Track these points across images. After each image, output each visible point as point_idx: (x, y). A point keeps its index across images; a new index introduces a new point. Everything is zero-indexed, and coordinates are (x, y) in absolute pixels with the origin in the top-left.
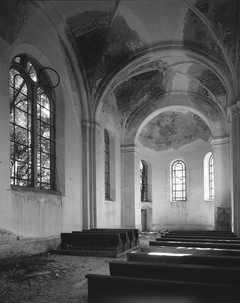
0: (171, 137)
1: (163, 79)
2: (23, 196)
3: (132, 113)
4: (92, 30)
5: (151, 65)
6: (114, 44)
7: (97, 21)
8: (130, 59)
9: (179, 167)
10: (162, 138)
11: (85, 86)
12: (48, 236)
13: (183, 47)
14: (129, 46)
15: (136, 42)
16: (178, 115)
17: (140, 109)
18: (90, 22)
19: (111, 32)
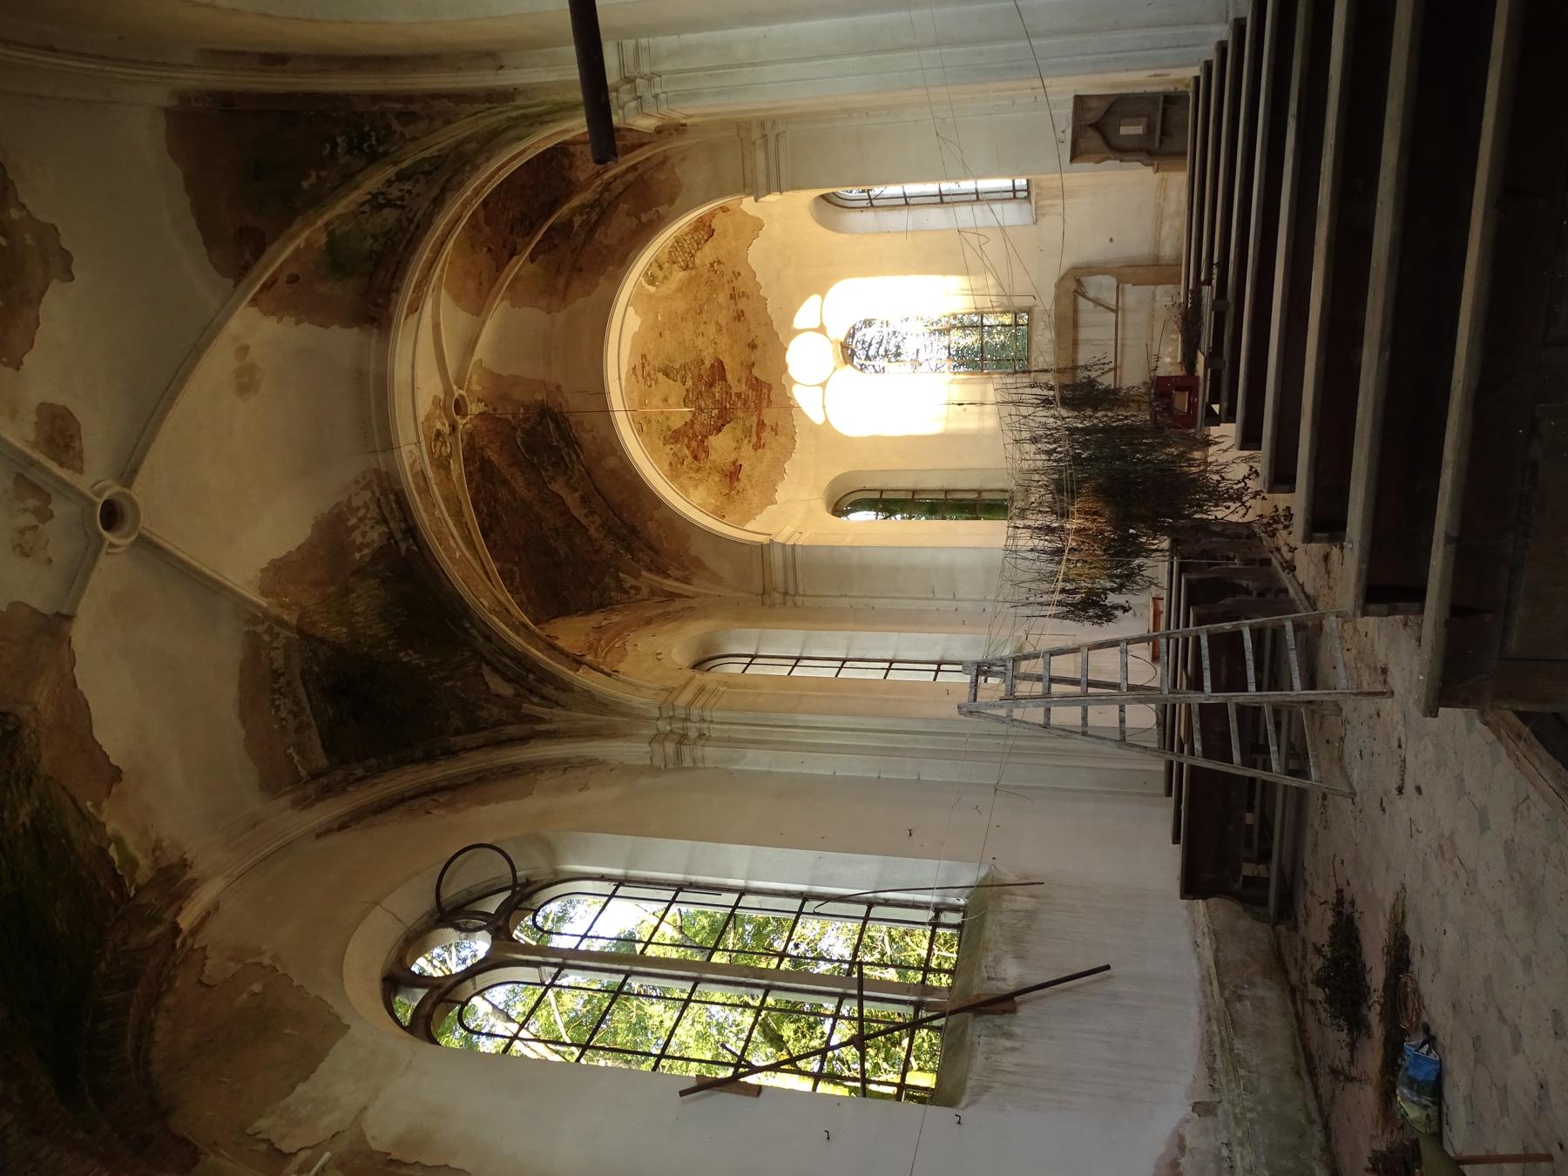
0: (736, 380)
2: (987, 1059)
3: (629, 550)
4: (304, 698)
5: (442, 464)
6: (359, 609)
7: (274, 672)
8: (414, 548)
11: (511, 741)
12: (1194, 962)
13: (379, 328)
14: (365, 552)
15: (353, 521)
16: (646, 352)
17: (611, 513)
18: (277, 702)
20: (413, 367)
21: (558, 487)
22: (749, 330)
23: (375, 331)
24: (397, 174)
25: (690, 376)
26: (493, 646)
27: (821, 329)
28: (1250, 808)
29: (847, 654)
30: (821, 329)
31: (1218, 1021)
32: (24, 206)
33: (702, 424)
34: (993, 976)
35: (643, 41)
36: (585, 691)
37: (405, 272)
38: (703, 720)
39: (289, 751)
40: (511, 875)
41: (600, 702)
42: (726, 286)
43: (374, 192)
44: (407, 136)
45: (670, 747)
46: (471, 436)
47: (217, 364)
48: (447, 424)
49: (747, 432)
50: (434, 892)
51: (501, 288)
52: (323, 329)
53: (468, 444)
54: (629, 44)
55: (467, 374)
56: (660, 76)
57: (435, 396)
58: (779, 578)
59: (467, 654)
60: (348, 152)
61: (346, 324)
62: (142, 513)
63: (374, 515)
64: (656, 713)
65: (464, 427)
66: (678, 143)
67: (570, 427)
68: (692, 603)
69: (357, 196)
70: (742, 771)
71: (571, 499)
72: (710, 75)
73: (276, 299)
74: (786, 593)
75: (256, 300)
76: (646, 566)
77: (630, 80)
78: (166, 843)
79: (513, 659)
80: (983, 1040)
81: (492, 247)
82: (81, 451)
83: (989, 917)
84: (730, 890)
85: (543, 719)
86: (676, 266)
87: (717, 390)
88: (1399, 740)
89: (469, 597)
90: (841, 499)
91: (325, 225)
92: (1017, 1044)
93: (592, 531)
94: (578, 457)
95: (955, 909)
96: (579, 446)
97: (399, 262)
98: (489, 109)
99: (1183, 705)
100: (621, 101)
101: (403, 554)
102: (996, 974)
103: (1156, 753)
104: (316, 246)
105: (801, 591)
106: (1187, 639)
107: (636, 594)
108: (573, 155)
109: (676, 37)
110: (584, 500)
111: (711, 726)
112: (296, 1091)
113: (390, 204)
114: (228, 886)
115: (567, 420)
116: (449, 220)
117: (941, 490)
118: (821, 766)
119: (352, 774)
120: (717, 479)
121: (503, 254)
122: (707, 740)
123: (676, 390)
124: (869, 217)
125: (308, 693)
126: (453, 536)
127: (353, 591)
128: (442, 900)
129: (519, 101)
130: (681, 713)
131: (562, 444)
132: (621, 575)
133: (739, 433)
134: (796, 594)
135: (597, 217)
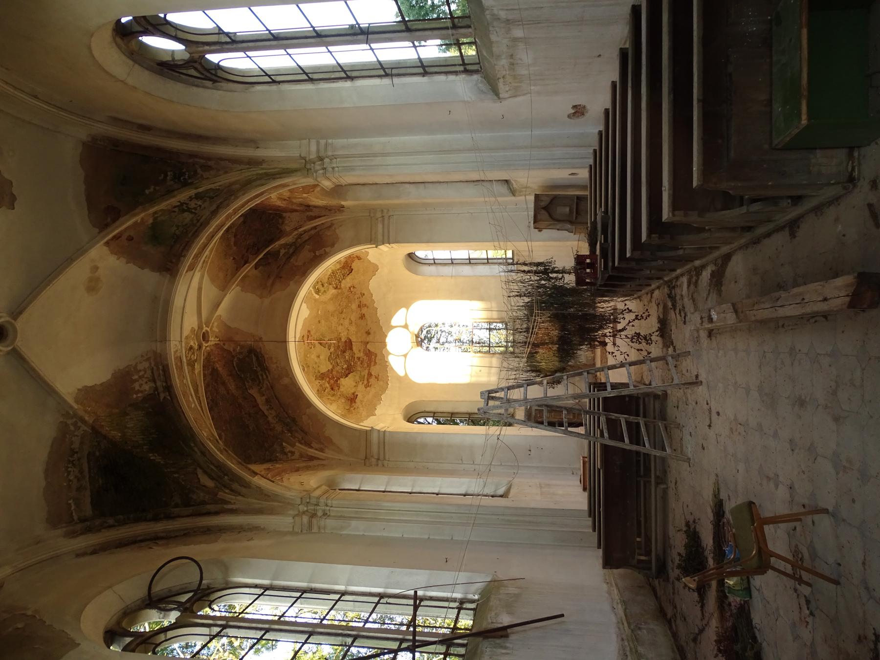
1: (225, 347)
3: (290, 431)
4: (87, 470)
8: (169, 398)
9: (411, 644)
10: (359, 372)
11: (209, 514)
15: (135, 377)
18: (69, 469)
19: (103, 426)
20: (185, 300)
21: (253, 392)
22: (367, 325)
23: (169, 276)
24: (196, 194)
26: (205, 458)
27: (406, 326)
28: (639, 536)
29: (412, 490)
30: (406, 326)
31: (628, 641)
33: (337, 372)
34: (495, 621)
35: (330, 141)
36: (257, 487)
37: (190, 247)
38: (327, 505)
39: (70, 502)
41: (266, 495)
43: (182, 201)
44: (205, 177)
45: (305, 519)
46: (209, 354)
47: (78, 271)
48: (197, 344)
49: (362, 378)
53: (206, 358)
54: (323, 142)
55: (211, 321)
56: (336, 159)
57: (193, 328)
59: (190, 461)
61: (153, 269)
62: (19, 335)
63: (149, 376)
64: (298, 501)
65: (206, 348)
66: (339, 217)
67: (264, 360)
69: (173, 201)
70: (349, 535)
71: (260, 400)
72: (361, 160)
73: (119, 245)
74: (378, 459)
75: (108, 243)
76: (299, 441)
77: (321, 159)
79: (216, 467)
80: (488, 650)
81: (236, 257)
83: (493, 596)
84: (335, 592)
85: (230, 502)
86: (331, 286)
87: (347, 355)
88: (707, 401)
90: (412, 416)
91: (154, 213)
92: (508, 652)
93: (270, 418)
94: (267, 377)
95: (472, 601)
97: (188, 242)
100: (316, 169)
101: (161, 400)
102: (496, 621)
103: (584, 437)
105: (387, 458)
106: (594, 399)
107: (291, 456)
108: (284, 218)
109: (346, 140)
110: (267, 401)
111: (331, 508)
113: (189, 210)
114: (13, 574)
115: (264, 357)
116: (219, 224)
117: (467, 413)
118: (395, 532)
120: (343, 401)
121: (241, 262)
122: (328, 516)
123: (325, 353)
124: (433, 268)
125: (89, 468)
126: (192, 396)
128: (152, 592)
130: (313, 501)
131: (259, 369)
133: (357, 378)
134: (385, 459)
135: (293, 251)
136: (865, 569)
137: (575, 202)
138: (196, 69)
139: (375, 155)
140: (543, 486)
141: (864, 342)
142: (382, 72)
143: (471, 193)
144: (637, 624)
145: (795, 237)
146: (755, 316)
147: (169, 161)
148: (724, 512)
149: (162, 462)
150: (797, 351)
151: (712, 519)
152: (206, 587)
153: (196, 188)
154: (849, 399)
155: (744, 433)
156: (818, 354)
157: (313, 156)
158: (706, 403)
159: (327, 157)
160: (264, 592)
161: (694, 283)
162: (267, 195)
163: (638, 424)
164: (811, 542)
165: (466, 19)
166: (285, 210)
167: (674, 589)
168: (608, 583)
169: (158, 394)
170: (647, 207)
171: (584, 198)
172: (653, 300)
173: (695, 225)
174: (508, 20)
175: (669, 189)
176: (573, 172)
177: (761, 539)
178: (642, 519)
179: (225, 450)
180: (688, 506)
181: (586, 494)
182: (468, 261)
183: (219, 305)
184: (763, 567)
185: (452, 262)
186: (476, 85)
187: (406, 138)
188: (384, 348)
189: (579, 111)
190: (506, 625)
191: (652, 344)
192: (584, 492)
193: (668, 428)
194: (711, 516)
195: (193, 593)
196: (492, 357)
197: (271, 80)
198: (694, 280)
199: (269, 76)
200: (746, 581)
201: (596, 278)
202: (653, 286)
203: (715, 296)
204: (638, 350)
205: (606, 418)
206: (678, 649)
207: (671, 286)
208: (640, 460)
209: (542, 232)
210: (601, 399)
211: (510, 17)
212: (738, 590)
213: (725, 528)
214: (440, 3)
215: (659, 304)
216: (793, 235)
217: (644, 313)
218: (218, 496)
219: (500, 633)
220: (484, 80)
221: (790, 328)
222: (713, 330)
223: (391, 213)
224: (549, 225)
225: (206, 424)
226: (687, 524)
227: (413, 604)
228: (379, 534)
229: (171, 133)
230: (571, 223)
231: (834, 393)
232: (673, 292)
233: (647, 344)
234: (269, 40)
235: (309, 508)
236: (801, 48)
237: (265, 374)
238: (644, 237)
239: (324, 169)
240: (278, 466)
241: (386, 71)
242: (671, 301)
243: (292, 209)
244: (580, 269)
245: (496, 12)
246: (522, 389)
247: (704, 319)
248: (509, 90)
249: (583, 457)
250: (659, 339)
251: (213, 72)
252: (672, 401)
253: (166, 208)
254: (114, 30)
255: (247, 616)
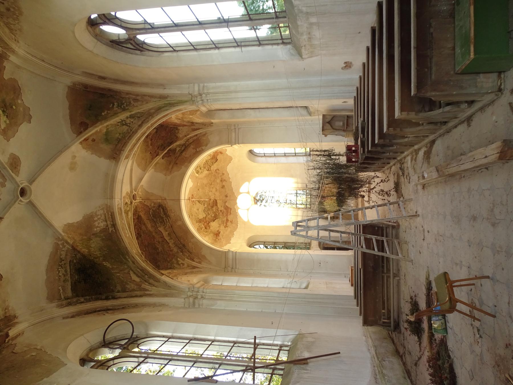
1: (145, 203)
3: (182, 252)
4: (69, 270)
7: (61, 259)
8: (114, 231)
11: (136, 296)
13: (116, 161)
17: (177, 240)
18: (59, 270)
20: (123, 175)
21: (161, 229)
23: (114, 162)
24: (130, 115)
25: (206, 203)
28: (384, 309)
30: (248, 193)
31: (377, 367)
32: (23, 100)
33: (209, 218)
35: (206, 84)
36: (164, 282)
38: (203, 292)
39: (59, 288)
40: (131, 334)
42: (220, 177)
43: (122, 119)
45: (191, 300)
47: (65, 159)
49: (223, 222)
50: (103, 336)
51: (152, 165)
52: (99, 158)
53: (135, 209)
54: (201, 85)
57: (127, 192)
58: (230, 262)
59: (126, 267)
60: (117, 107)
61: (106, 158)
63: (103, 218)
64: (187, 290)
66: (210, 129)
67: (167, 211)
68: (201, 270)
70: (215, 309)
71: (165, 234)
74: (232, 268)
77: (201, 95)
78: (10, 308)
79: (141, 270)
80: (296, 371)
82: (20, 170)
84: (208, 340)
85: (148, 290)
87: (214, 208)
89: (129, 248)
93: (170, 244)
96: (170, 218)
97: (125, 142)
98: (159, 100)
99: (360, 252)
101: (110, 232)
104: (102, 132)
105: (237, 268)
106: (358, 225)
111: (206, 294)
112: (43, 380)
113: (126, 124)
114: (29, 327)
117: (283, 242)
118: (242, 308)
119: (80, 300)
120: (212, 235)
123: (201, 207)
124: (264, 159)
125: (70, 269)
127: (92, 240)
128: (105, 339)
129: (168, 99)
130: (196, 290)
131: (164, 216)
132: (178, 259)
133: (220, 222)
134: (236, 268)
136: (509, 306)
137: (346, 118)
138: (131, 44)
139: (231, 92)
140: (328, 283)
141: (508, 179)
142: (235, 44)
143: (285, 114)
144: (383, 358)
145: (470, 126)
146: (448, 172)
147: (115, 97)
148: (432, 288)
149: (110, 267)
150: (472, 189)
151: (425, 292)
152: (136, 337)
153: (130, 112)
154: (500, 213)
155: (443, 241)
156: (483, 190)
157: (196, 93)
158: (421, 226)
159: (204, 94)
160: (168, 340)
161: (414, 159)
162: (170, 116)
163: (383, 241)
164: (480, 296)
165: (283, 13)
166: (180, 125)
167: (404, 337)
168: (365, 336)
169: (108, 228)
170: (387, 112)
171: (351, 117)
172: (391, 172)
173: (414, 121)
174: (308, 13)
175: (399, 100)
176: (345, 101)
177: (451, 293)
178: (385, 298)
179: (146, 260)
180: (411, 288)
181: (353, 288)
182: (284, 155)
183: (142, 179)
184: (452, 309)
185: (275, 155)
186: (289, 51)
187: (250, 82)
188: (235, 205)
189: (348, 65)
190: (306, 357)
191: (390, 196)
192: (352, 287)
193: (400, 244)
194: (424, 291)
195: (128, 340)
196: (298, 210)
197: (173, 50)
198: (414, 157)
199: (172, 47)
200: (444, 324)
201: (358, 158)
202: (391, 164)
203: (426, 165)
204: (383, 199)
205: (365, 238)
206: (406, 372)
207: (402, 163)
208: (384, 266)
209: (327, 137)
210: (361, 225)
211: (309, 11)
212: (440, 330)
213: (433, 296)
214: (267, 8)
215: (395, 174)
216: (469, 125)
217: (386, 179)
218: (142, 287)
219: (304, 362)
220: (293, 48)
221: (468, 177)
222: (425, 184)
223: (240, 127)
224: (331, 132)
225: (135, 246)
226: (411, 298)
227: (253, 347)
228: (233, 309)
229: (117, 81)
230: (344, 131)
231: (492, 210)
232: (403, 166)
233: (388, 196)
234: (172, 27)
235: (193, 293)
236: (470, 16)
237: (168, 219)
238: (385, 130)
239: (202, 100)
240: (175, 271)
241: (238, 44)
242: (402, 171)
243: (183, 125)
244: (349, 153)
245: (300, 8)
246: (316, 221)
247: (420, 178)
248: (308, 53)
249: (351, 267)
250: (395, 193)
251: (141, 45)
252: (402, 228)
253: (113, 123)
254: (87, 22)
255: (158, 352)
